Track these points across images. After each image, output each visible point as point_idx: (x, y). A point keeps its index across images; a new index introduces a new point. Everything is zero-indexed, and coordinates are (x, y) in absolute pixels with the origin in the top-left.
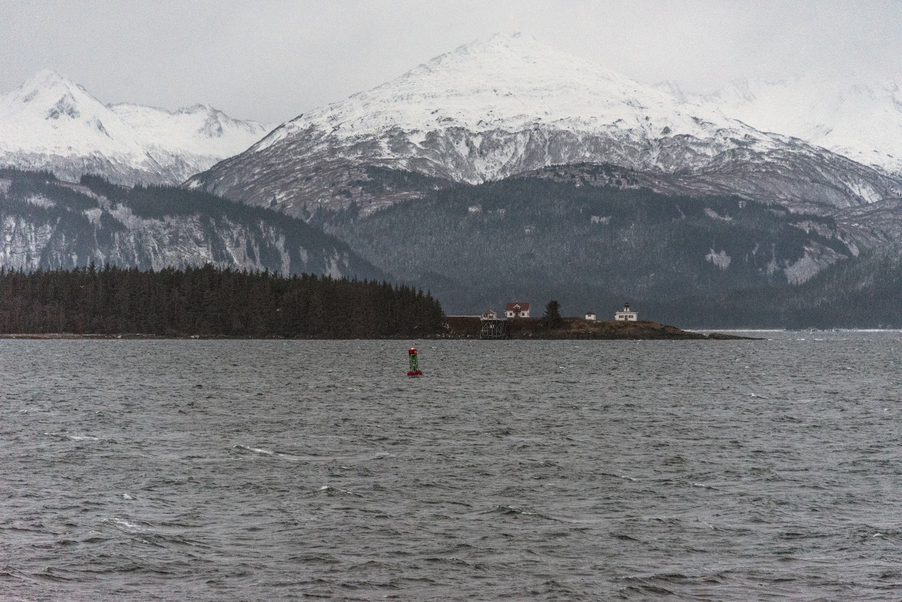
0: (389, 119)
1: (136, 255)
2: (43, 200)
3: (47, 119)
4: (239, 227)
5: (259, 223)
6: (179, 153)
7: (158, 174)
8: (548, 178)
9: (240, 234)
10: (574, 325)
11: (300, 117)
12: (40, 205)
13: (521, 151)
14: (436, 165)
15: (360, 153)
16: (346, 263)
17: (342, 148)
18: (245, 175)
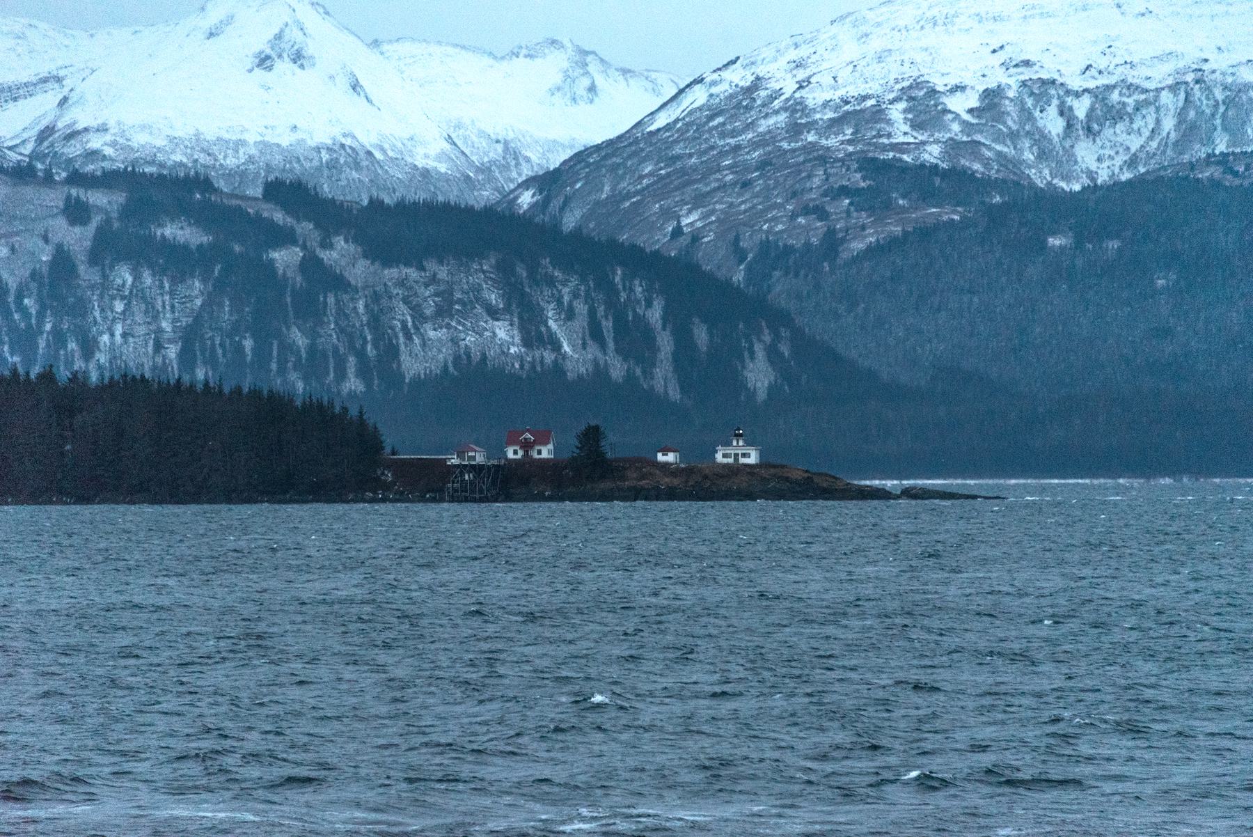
0: (907, 65)
1: (369, 338)
2: (188, 231)
3: (250, 71)
4: (574, 281)
5: (614, 273)
6: (511, 136)
7: (468, 177)
8: (1211, 179)
9: (575, 295)
10: (633, 474)
11: (733, 62)
12: (182, 241)
13: (1169, 124)
14: (999, 154)
15: (849, 131)
16: (785, 349)
17: (816, 122)
18: (622, 178)
